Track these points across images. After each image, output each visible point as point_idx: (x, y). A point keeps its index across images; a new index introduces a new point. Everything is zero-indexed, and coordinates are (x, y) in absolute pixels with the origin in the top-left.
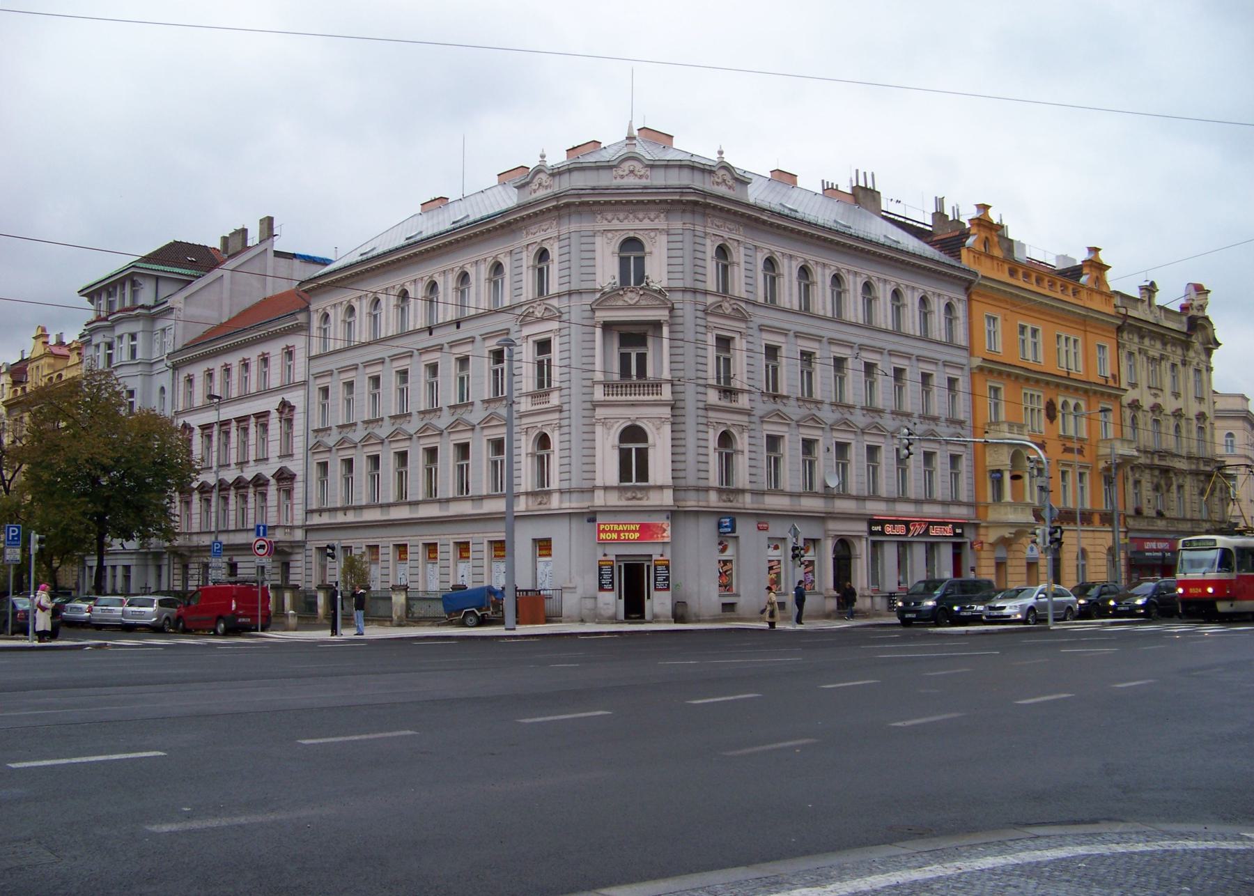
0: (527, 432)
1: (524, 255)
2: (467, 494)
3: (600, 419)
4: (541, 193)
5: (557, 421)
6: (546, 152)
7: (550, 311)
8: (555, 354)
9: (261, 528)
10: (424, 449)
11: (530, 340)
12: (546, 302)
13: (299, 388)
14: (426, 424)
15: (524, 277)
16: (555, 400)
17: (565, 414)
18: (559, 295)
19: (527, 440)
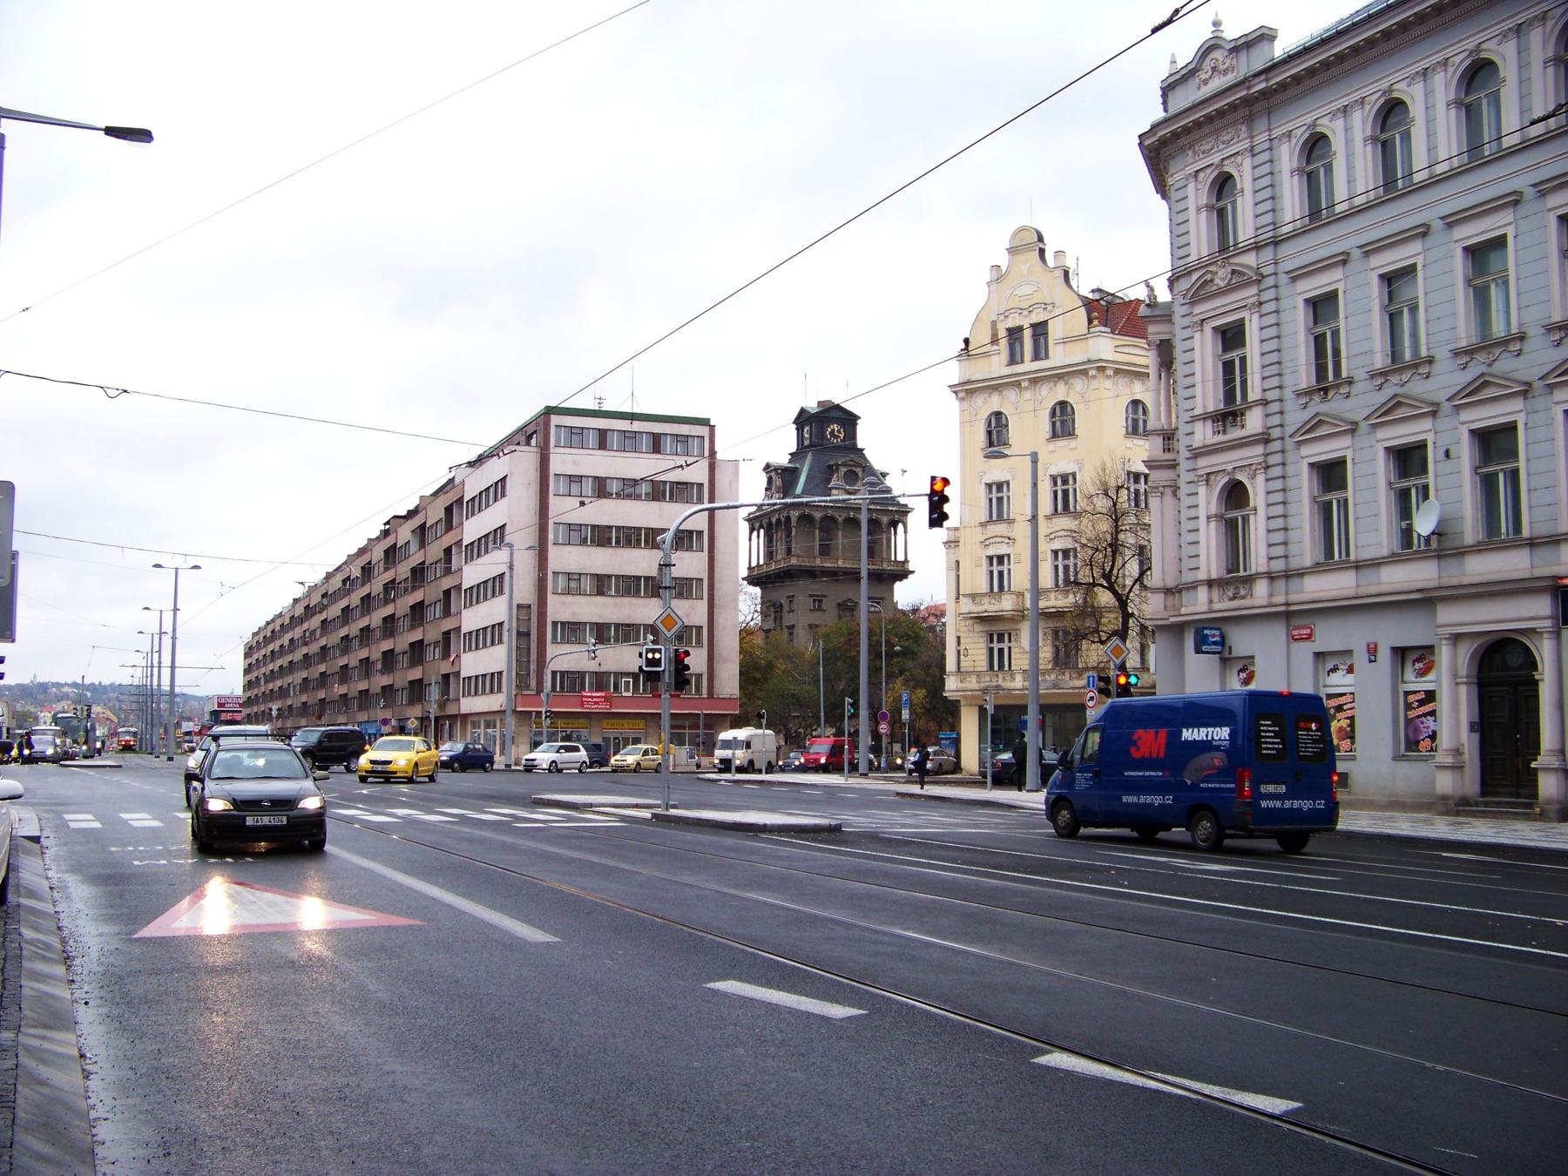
0: (1207, 480)
1: (1191, 186)
2: (1245, 570)
3: (1157, 488)
4: (1218, 83)
5: (1261, 459)
6: (1221, 17)
7: (1241, 273)
8: (1253, 347)
9: (996, 668)
10: (1387, 449)
11: (1208, 328)
12: (1232, 261)
13: (1415, 239)
14: (1483, 375)
15: (1192, 226)
16: (1254, 422)
17: (1276, 446)
18: (1257, 247)
19: (1207, 495)
